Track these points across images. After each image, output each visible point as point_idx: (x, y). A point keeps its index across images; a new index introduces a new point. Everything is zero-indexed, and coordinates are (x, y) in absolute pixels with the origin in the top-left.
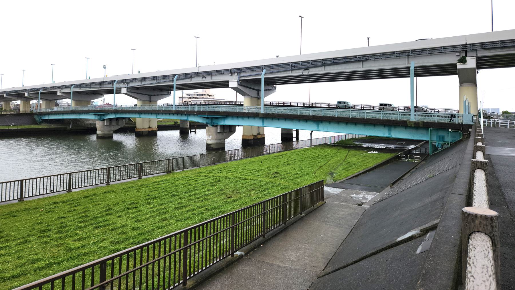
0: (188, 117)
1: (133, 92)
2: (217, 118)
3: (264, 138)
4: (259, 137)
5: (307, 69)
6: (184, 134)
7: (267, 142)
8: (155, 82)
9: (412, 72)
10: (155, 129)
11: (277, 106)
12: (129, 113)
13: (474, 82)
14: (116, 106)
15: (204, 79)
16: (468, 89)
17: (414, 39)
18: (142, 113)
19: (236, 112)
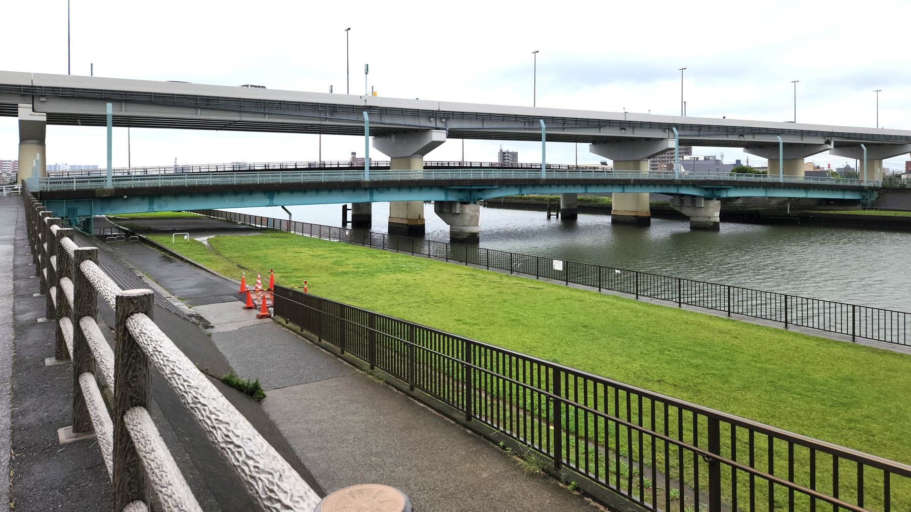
0: (521, 191)
1: (600, 143)
2: (480, 190)
3: (424, 225)
4: (419, 223)
5: (742, 135)
6: (569, 219)
7: (428, 229)
8: (696, 133)
9: (109, 121)
10: (645, 215)
11: (281, 170)
12: (598, 185)
13: (40, 139)
14: (548, 167)
15: (623, 131)
16: (32, 148)
17: (164, 79)
18: (590, 185)
19: (397, 181)
